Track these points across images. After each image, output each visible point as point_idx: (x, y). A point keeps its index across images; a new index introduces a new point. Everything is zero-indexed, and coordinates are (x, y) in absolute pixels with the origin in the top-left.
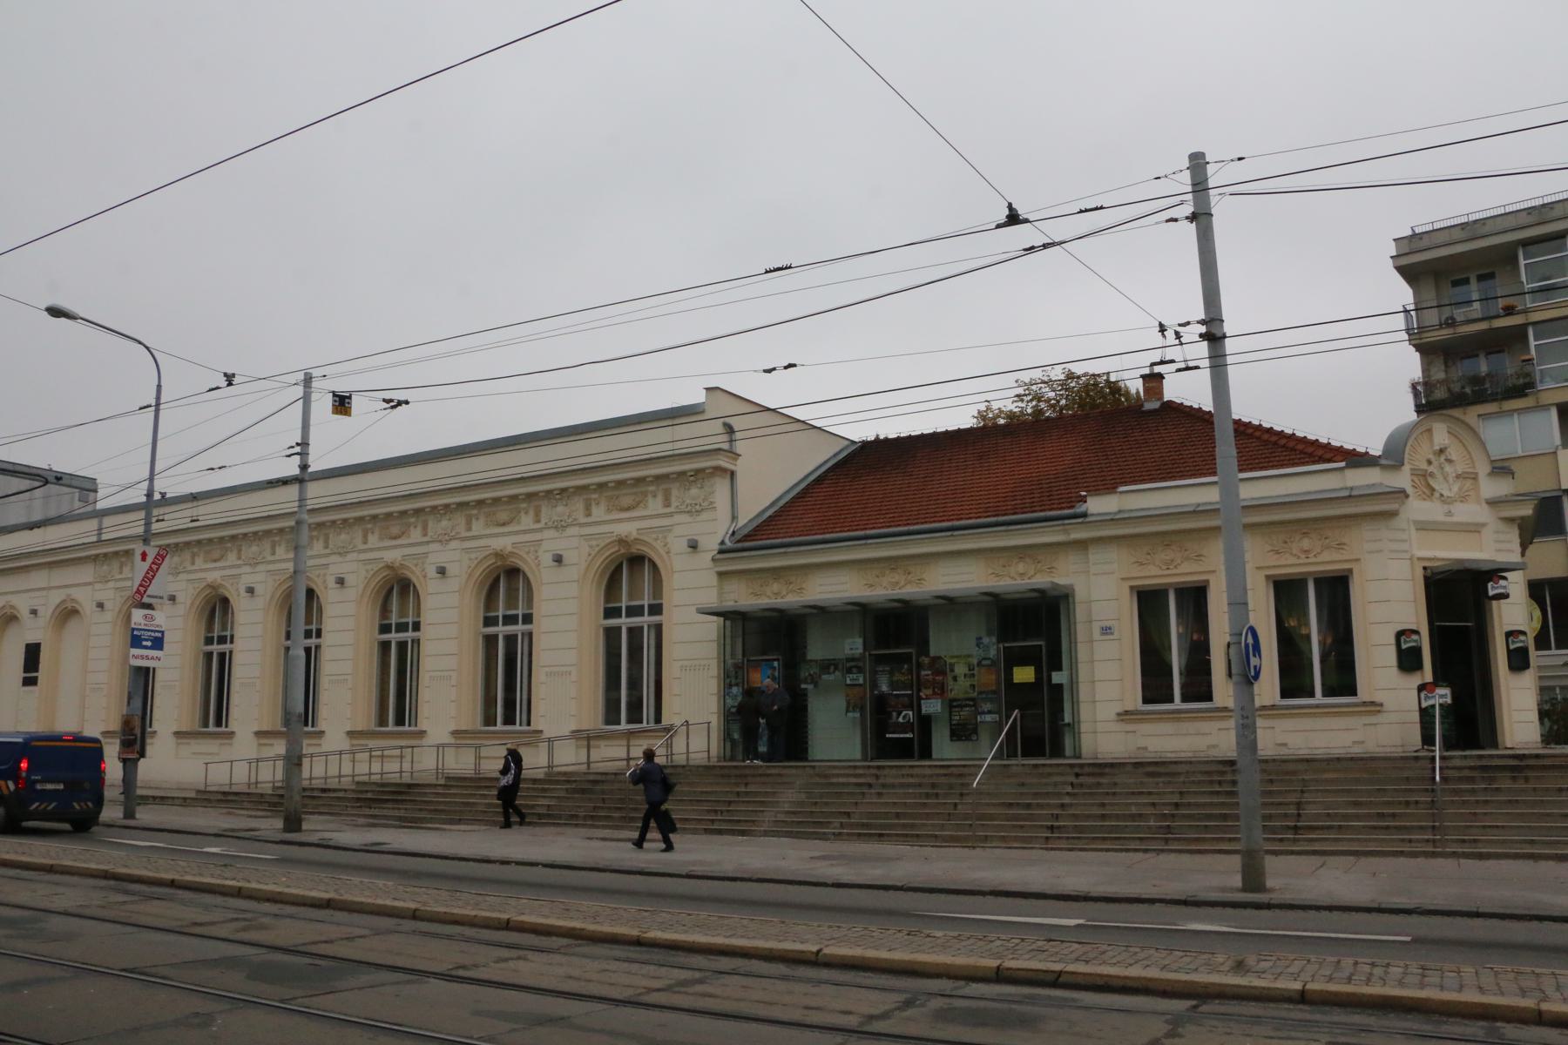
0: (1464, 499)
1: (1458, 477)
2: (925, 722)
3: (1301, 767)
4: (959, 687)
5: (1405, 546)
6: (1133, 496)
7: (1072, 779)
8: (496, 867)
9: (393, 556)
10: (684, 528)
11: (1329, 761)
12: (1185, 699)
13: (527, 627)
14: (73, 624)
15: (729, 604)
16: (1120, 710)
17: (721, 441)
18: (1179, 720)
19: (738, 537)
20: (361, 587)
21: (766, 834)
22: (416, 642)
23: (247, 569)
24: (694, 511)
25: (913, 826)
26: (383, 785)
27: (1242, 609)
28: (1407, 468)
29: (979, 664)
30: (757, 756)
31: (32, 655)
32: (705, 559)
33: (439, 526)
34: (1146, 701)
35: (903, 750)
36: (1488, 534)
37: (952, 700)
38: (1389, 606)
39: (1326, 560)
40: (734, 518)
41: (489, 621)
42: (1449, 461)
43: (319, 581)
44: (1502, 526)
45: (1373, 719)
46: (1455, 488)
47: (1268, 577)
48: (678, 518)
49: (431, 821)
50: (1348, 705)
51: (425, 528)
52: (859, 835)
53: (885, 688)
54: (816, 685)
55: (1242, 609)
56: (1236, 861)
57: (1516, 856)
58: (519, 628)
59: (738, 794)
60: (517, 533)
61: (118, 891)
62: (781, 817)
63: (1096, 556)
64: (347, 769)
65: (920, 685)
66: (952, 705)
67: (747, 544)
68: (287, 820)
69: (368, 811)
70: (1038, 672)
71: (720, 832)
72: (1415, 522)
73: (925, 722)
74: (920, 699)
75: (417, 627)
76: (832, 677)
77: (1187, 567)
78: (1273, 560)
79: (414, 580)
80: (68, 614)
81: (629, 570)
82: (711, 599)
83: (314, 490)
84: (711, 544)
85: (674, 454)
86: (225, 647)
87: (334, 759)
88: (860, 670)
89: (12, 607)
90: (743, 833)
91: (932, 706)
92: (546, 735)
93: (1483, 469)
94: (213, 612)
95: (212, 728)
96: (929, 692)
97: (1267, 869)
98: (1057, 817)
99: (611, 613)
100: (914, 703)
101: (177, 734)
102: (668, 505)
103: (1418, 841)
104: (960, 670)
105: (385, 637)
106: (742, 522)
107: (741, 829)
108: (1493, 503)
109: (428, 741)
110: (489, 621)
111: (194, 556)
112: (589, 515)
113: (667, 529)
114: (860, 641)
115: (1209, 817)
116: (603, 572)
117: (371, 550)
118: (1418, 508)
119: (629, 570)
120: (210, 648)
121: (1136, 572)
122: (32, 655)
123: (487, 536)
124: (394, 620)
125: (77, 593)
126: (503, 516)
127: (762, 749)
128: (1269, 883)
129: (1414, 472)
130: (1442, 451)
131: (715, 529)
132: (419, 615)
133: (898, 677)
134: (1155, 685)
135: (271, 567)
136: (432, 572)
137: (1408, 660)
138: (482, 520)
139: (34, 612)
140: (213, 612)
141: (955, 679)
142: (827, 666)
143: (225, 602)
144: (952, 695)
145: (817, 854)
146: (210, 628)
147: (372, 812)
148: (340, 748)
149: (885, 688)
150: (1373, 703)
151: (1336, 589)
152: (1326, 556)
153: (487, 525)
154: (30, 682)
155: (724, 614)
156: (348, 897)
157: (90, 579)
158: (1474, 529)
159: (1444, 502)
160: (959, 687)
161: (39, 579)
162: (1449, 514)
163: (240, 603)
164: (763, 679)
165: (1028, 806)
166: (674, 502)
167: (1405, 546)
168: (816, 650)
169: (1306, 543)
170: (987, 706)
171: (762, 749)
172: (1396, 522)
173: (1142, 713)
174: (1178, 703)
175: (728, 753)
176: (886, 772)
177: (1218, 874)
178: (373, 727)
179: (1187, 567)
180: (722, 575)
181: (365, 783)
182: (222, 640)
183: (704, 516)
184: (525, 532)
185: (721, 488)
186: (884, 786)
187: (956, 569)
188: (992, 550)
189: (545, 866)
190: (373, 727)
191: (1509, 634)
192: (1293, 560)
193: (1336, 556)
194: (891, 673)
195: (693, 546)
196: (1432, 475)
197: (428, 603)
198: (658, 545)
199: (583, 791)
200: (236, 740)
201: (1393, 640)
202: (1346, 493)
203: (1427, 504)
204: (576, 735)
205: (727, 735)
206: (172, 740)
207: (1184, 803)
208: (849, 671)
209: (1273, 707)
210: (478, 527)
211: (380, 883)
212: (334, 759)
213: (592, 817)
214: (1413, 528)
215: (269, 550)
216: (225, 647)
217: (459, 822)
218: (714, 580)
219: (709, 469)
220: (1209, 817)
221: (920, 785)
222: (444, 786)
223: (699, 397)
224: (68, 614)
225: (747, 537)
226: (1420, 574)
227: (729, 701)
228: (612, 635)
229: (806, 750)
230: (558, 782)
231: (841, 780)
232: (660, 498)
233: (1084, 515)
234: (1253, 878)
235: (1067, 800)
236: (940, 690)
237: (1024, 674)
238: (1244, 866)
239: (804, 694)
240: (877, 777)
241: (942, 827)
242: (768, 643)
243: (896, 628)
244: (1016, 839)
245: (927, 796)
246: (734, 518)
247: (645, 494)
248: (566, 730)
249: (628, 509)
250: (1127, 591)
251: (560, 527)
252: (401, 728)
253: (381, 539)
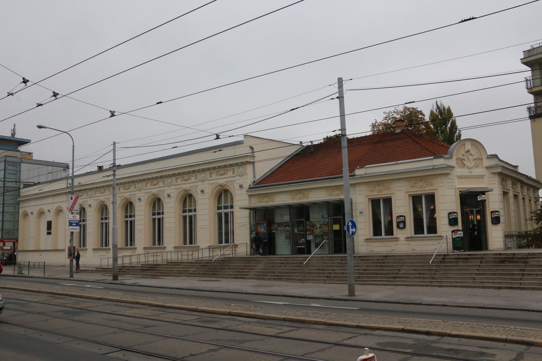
0: (477, 166)
1: (474, 160)
2: (308, 243)
3: (406, 258)
4: (317, 231)
5: (453, 184)
6: (369, 169)
7: (340, 261)
8: (165, 289)
9: (222, 181)
10: (239, 181)
11: (414, 256)
12: (386, 235)
13: (231, 210)
14: (61, 214)
15: (253, 205)
16: (406, 237)
17: (250, 151)
18: (382, 241)
19: (256, 183)
20: (210, 193)
21: (250, 278)
22: (195, 215)
23: (89, 199)
24: (241, 175)
25: (290, 276)
26: (149, 265)
27: (402, 207)
28: (454, 157)
29: (323, 224)
30: (259, 254)
31: (49, 224)
32: (244, 191)
33: (201, 176)
34: (415, 233)
35: (300, 251)
36: (486, 178)
37: (315, 236)
38: (447, 203)
39: (384, 194)
40: (254, 177)
41: (219, 208)
42: (471, 155)
43: (133, 199)
44: (491, 175)
45: (396, 243)
46: (473, 164)
47: (409, 195)
48: (237, 178)
49: (160, 276)
50: (433, 237)
51: (196, 177)
52: (275, 279)
53: (296, 232)
54: (277, 230)
55: (402, 207)
56: (346, 287)
57: (450, 286)
58: (229, 210)
59: (246, 266)
60: (227, 178)
61: (51, 297)
62: (256, 273)
63: (358, 188)
64: (169, 257)
65: (307, 230)
66: (315, 237)
67: (259, 185)
68: (114, 276)
69: (143, 273)
70: (340, 226)
71: (238, 278)
72: (457, 176)
73: (308, 243)
74: (306, 235)
75: (195, 210)
76: (281, 228)
77: (427, 188)
78: (411, 189)
79: (192, 193)
80: (59, 211)
81: (223, 195)
82: (246, 204)
83: (120, 174)
84: (246, 186)
85: (223, 159)
86: (132, 219)
87: (169, 254)
88: (289, 226)
89: (60, 207)
90: (243, 278)
91: (310, 238)
92: (201, 247)
93: (484, 157)
94: (155, 204)
95: (104, 247)
96: (309, 233)
97: (355, 289)
98: (330, 273)
99: (184, 211)
100: (304, 236)
101: (94, 249)
102: (234, 174)
103: (427, 281)
104: (318, 226)
105: (185, 214)
106: (258, 177)
107: (243, 277)
108: (487, 168)
109: (167, 250)
110: (219, 208)
111: (96, 192)
112: (211, 177)
113: (234, 181)
114: (289, 217)
115: (372, 274)
116: (216, 196)
117: (213, 180)
118: (459, 171)
119: (223, 195)
120: (102, 221)
121: (411, 189)
122: (49, 224)
123: (217, 179)
124: (223, 205)
125: (43, 207)
126: (222, 172)
127: (261, 251)
128: (356, 293)
129: (457, 159)
130: (468, 151)
131: (248, 180)
132: (232, 203)
133: (300, 228)
134: (377, 231)
135: (176, 187)
136: (199, 192)
137: (453, 222)
138: (215, 174)
139: (49, 211)
140: (155, 204)
141: (316, 229)
142: (280, 224)
143: (131, 203)
144: (316, 234)
145: (252, 284)
146: (102, 215)
147: (145, 273)
148: (141, 252)
149: (296, 232)
150: (440, 236)
151: (431, 198)
152: (427, 188)
153: (217, 176)
154: (49, 233)
155: (250, 209)
156: (106, 297)
157: (65, 200)
158: (481, 177)
159: (469, 169)
160: (317, 231)
161: (50, 200)
162: (471, 172)
163: (137, 204)
164: (262, 229)
165: (324, 270)
166: (236, 173)
167: (453, 184)
168: (278, 219)
169: (421, 184)
170: (326, 237)
171: (261, 251)
172: (449, 176)
173: (374, 239)
174: (426, 234)
175: (253, 252)
176: (290, 259)
177: (341, 290)
178: (152, 246)
179: (385, 192)
180: (250, 196)
181: (144, 264)
182: (131, 216)
183: (244, 177)
184: (160, 187)
185: (249, 168)
186: (287, 263)
187: (318, 194)
188: (328, 187)
189: (176, 289)
190: (152, 246)
191: (492, 212)
192: (417, 190)
193: (430, 188)
194: (298, 227)
195: (241, 186)
196: (464, 159)
197: (165, 206)
198: (231, 186)
199: (204, 266)
200: (88, 252)
201: (447, 216)
202: (431, 168)
203: (463, 170)
204: (209, 248)
205: (251, 247)
206: (92, 252)
207: (386, 269)
208: (286, 226)
209: (411, 237)
210: (214, 176)
211: (117, 293)
212: (169, 254)
213: (204, 274)
214: (456, 178)
215: (209, 176)
216: (132, 219)
217: (168, 276)
218: (247, 197)
219: (245, 162)
220: (372, 274)
221: (297, 263)
222: (166, 265)
223: (241, 138)
224: (59, 211)
225: (259, 183)
226: (458, 193)
227: (252, 236)
228: (220, 215)
229: (275, 252)
230: (198, 263)
231: (277, 262)
232: (231, 171)
233: (354, 175)
234: (352, 292)
235: (336, 268)
236: (312, 233)
237: (336, 227)
238: (349, 289)
239: (274, 234)
240: (286, 260)
241: (298, 276)
242: (263, 216)
243: (301, 212)
244: (316, 280)
245: (298, 266)
246: (254, 177)
247: (227, 170)
248: (206, 246)
249: (222, 175)
250: (367, 200)
251: (203, 181)
252: (191, 245)
253: (151, 185)
